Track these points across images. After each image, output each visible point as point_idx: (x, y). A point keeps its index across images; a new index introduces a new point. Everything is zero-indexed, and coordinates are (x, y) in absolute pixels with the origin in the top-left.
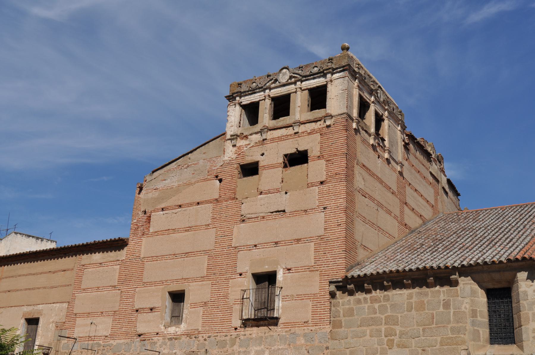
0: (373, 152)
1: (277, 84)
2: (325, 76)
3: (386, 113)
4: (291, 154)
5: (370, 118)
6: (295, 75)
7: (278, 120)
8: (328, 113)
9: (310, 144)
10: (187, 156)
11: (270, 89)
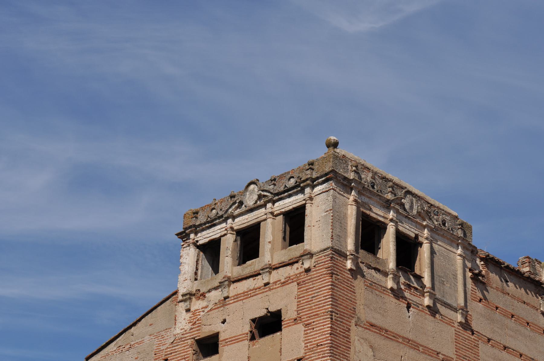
0: (395, 301)
1: (243, 208)
2: (302, 191)
3: (426, 231)
4: (260, 318)
5: (388, 247)
6: (265, 193)
7: (244, 265)
8: (305, 251)
9: (283, 300)
10: (129, 331)
11: (234, 218)
